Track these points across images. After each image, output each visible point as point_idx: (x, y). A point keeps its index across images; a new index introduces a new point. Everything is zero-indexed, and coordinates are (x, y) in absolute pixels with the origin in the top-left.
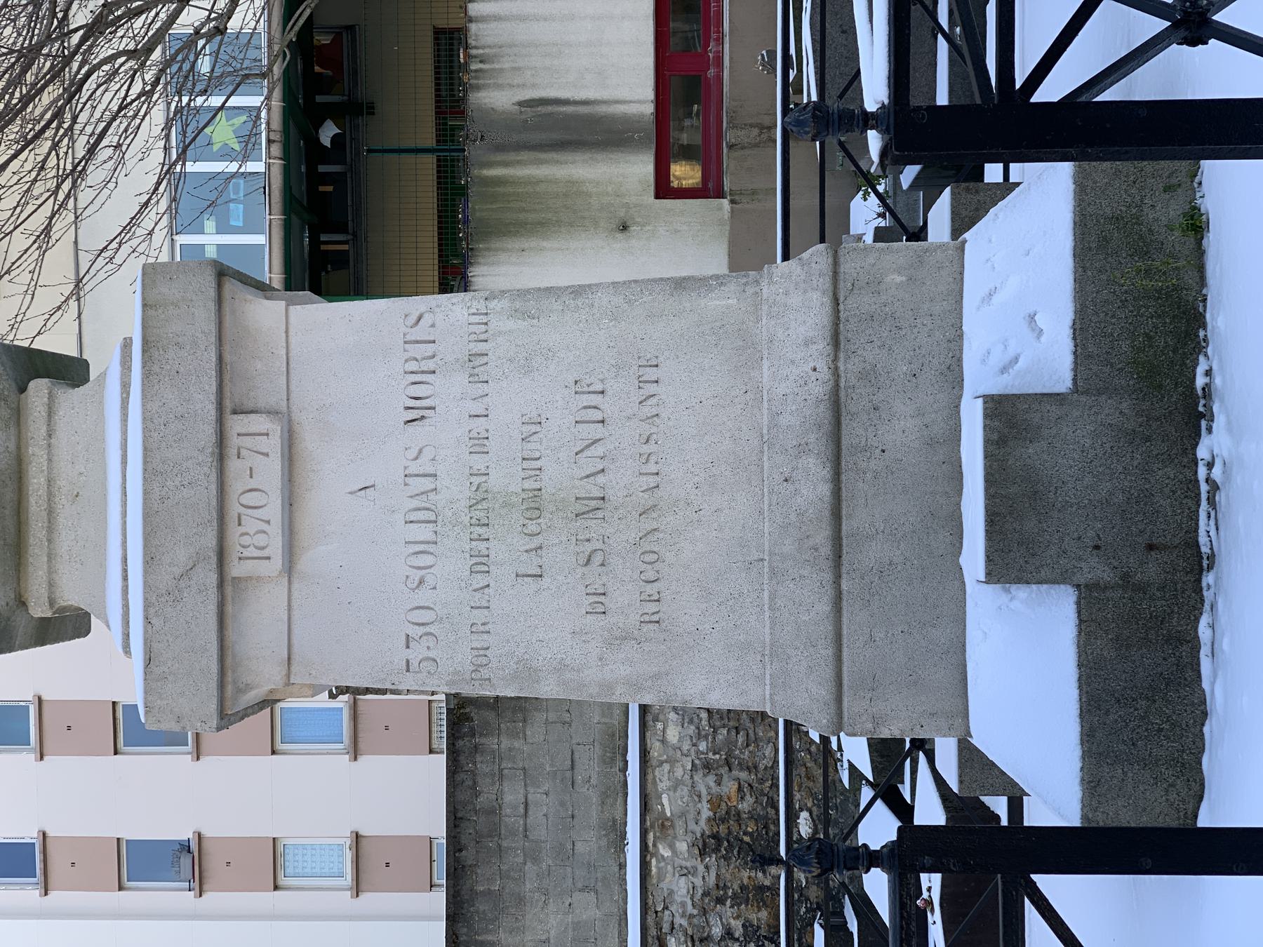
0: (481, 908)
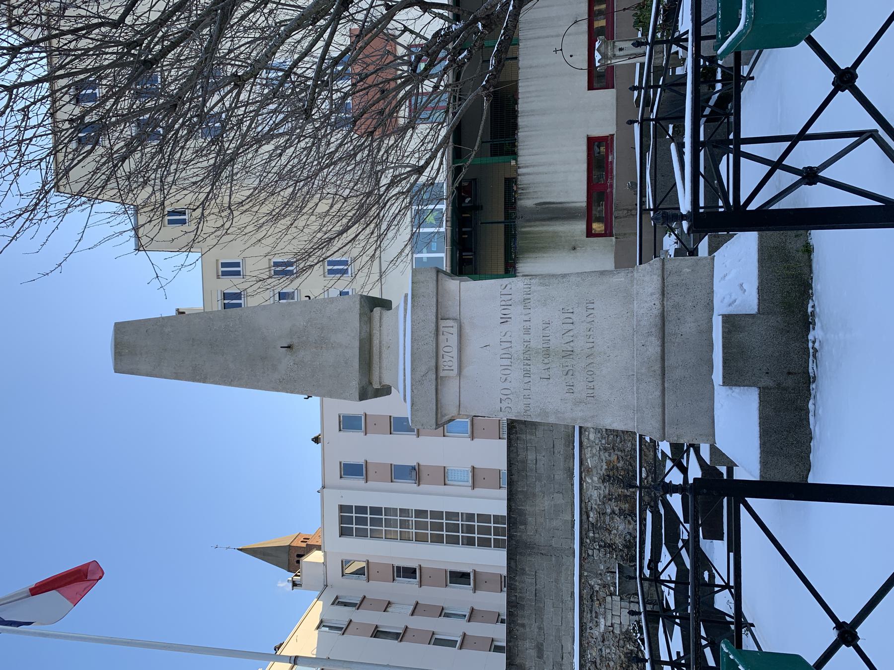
0: (520, 497)
